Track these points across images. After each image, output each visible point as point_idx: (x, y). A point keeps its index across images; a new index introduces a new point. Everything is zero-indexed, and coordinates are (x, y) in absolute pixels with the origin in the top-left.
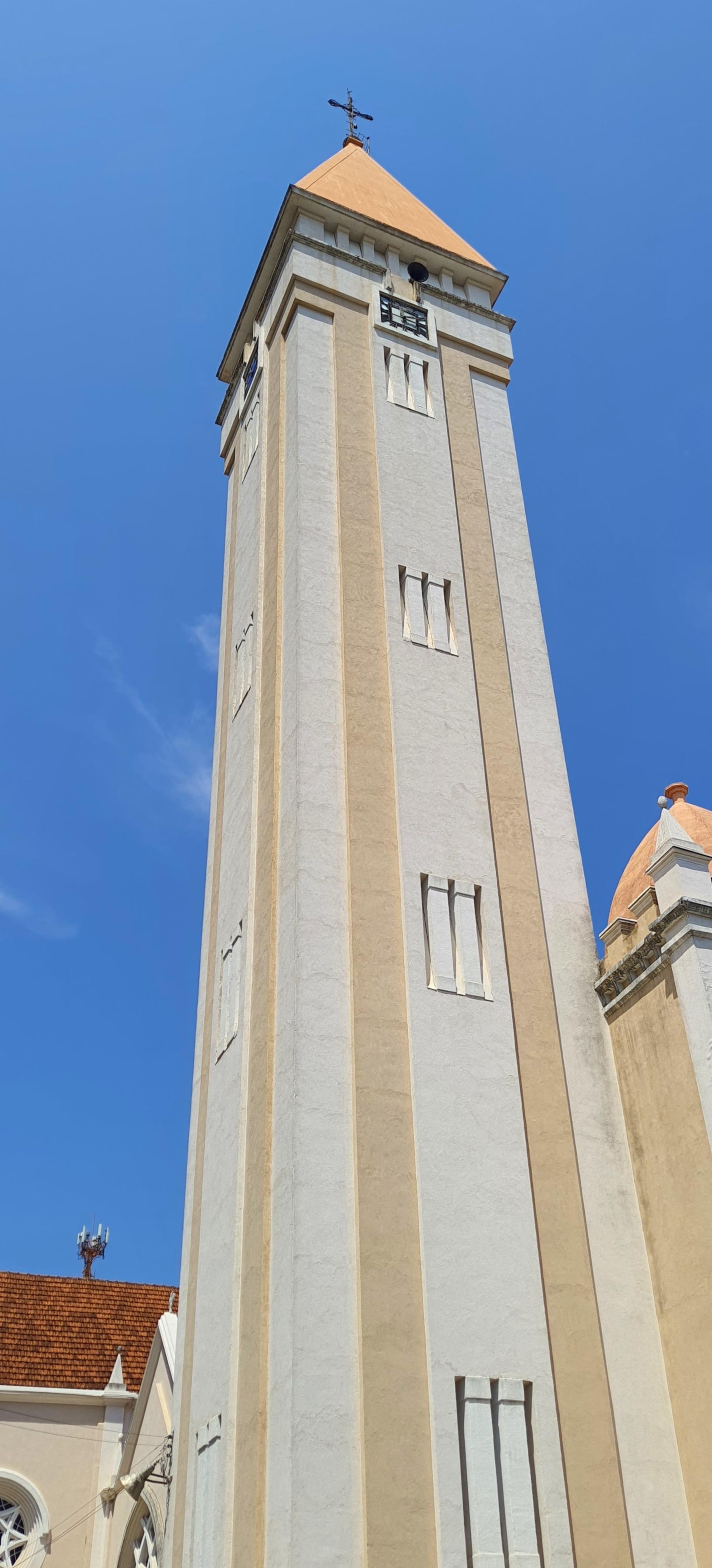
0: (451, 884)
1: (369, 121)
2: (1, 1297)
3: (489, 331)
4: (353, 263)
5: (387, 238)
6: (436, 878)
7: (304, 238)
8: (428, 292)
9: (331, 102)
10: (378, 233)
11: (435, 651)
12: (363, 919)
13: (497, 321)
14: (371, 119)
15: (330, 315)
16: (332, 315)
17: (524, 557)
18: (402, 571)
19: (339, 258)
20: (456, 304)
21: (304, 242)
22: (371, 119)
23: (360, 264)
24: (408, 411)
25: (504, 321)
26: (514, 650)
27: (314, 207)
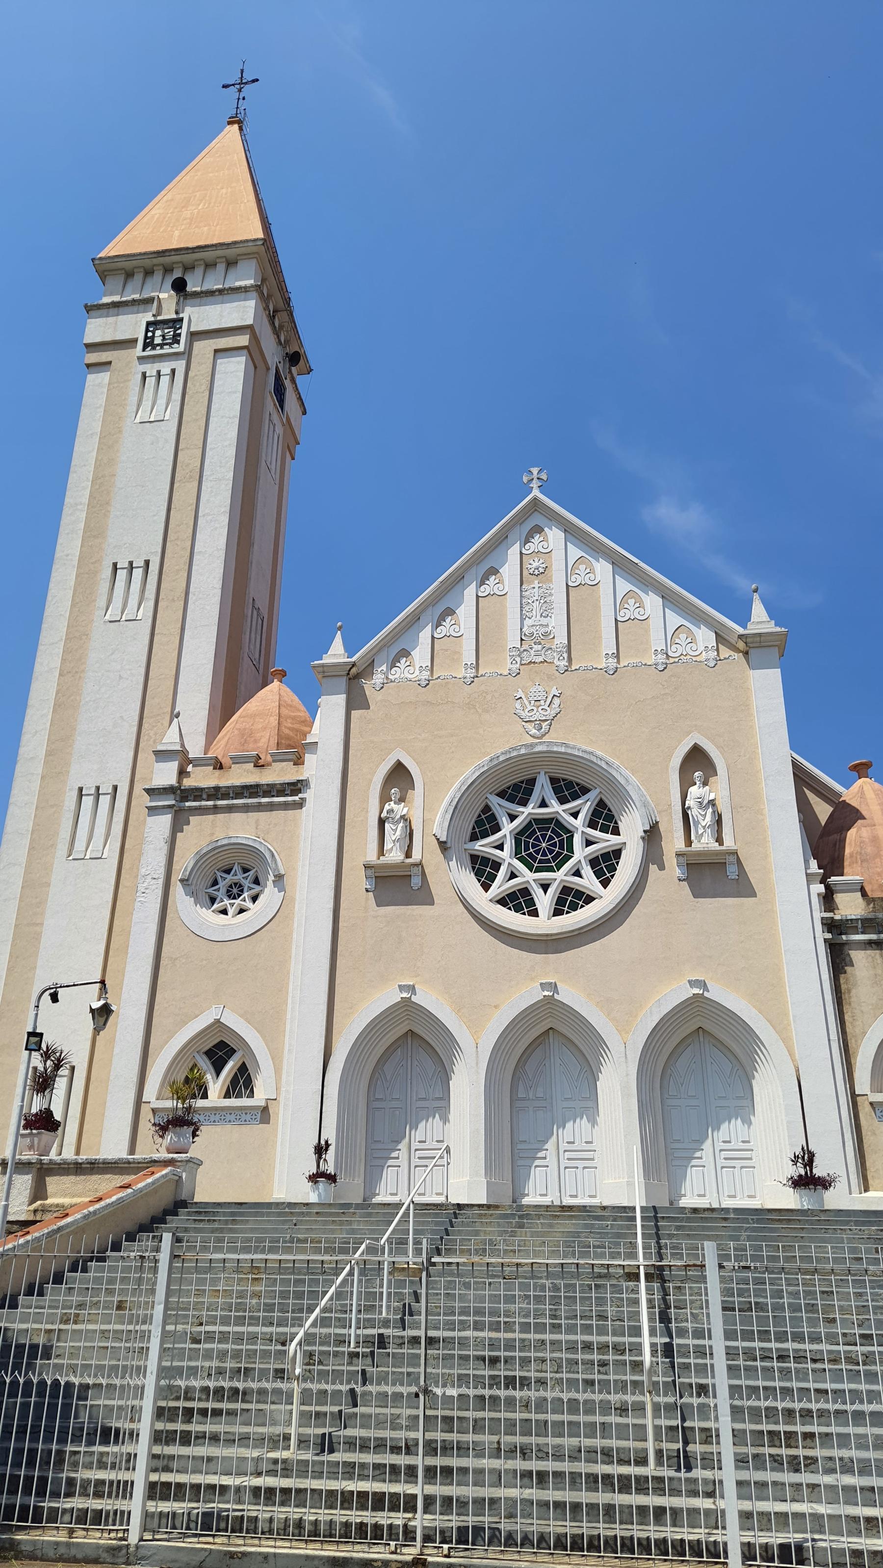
0: (98, 788)
1: (256, 83)
2: (879, 1419)
3: (236, 307)
4: (133, 305)
5: (167, 260)
6: (87, 788)
7: (94, 306)
8: (188, 297)
9: (225, 86)
10: (161, 260)
11: (109, 623)
12: (39, 825)
13: (246, 291)
14: (257, 80)
15: (106, 365)
16: (109, 363)
17: (223, 510)
18: (115, 565)
19: (122, 306)
20: (212, 295)
21: (95, 308)
22: (257, 80)
23: (137, 303)
24: (148, 424)
25: (251, 289)
26: (194, 595)
27: (113, 266)
